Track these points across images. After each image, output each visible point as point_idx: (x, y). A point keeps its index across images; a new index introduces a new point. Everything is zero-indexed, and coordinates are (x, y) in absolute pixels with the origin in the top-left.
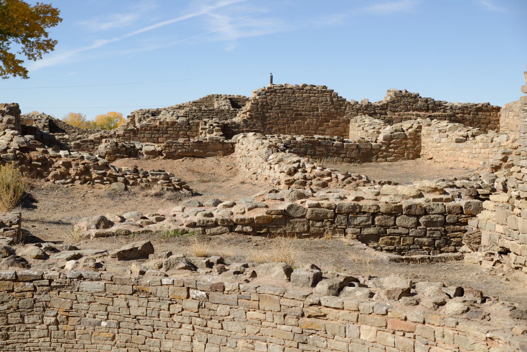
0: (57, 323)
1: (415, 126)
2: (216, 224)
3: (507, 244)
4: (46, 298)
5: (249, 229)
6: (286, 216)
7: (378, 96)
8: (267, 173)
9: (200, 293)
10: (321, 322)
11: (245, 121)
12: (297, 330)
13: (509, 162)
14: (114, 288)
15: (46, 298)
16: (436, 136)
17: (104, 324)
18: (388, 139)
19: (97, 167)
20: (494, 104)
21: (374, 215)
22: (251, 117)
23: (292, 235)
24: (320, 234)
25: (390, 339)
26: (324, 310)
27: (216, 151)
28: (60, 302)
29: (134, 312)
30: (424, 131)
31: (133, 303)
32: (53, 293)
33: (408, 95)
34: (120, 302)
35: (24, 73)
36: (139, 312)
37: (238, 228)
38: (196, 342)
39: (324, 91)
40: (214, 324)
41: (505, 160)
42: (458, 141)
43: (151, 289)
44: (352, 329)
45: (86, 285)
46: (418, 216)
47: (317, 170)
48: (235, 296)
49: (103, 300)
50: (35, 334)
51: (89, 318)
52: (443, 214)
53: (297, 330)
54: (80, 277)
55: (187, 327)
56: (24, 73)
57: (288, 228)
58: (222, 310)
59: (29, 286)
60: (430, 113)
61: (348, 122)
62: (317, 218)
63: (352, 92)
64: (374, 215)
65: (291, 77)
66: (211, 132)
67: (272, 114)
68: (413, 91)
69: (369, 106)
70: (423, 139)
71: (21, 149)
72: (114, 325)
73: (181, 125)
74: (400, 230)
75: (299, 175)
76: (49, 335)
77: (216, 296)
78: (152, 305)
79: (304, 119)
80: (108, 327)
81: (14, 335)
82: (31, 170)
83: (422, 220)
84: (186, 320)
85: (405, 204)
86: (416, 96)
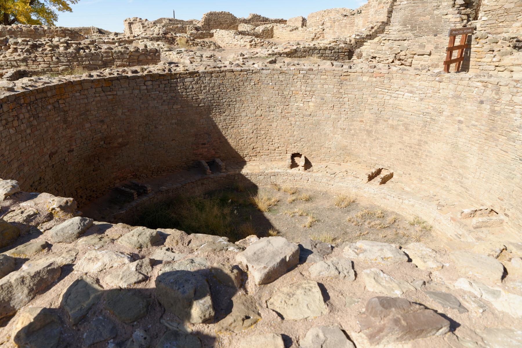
0: (255, 84)
1: (272, 26)
2: (276, 54)
3: (375, 55)
4: (251, 76)
5: (285, 55)
6: (296, 51)
7: (247, 17)
8: (236, 43)
9: (304, 72)
10: (348, 77)
11: (202, 26)
12: (340, 80)
13: (317, 37)
14: (274, 72)
15: (251, 76)
16: (281, 30)
17: (271, 84)
18: (263, 31)
19: (191, 40)
20: (285, 19)
21: (320, 50)
22: (205, 24)
23: (297, 57)
24: (305, 57)
25: (374, 79)
26: (349, 73)
27: (207, 36)
28: (256, 77)
29: (280, 79)
30: (275, 28)
31: (280, 77)
32: (254, 75)
33: (257, 16)
34: (276, 76)
35: (71, 10)
36: (282, 79)
37: (282, 55)
38: (302, 87)
39: (229, 14)
40: (309, 81)
41: (315, 36)
42: (290, 31)
43: (286, 72)
44: (360, 78)
45: (264, 71)
46: (332, 50)
47: (259, 41)
48: (317, 72)
49: (270, 76)
50: (248, 89)
51: (265, 82)
52: (338, 49)
53: (340, 80)
54: (263, 69)
55: (299, 83)
56: (71, 10)
57: (296, 55)
58: (312, 76)
59: (245, 73)
60: (265, 22)
61: (238, 26)
62: (305, 51)
63: (239, 15)
64: (320, 50)
65: (218, 9)
66: (192, 30)
67: (212, 23)
68: (259, 14)
69: (244, 20)
70: (274, 31)
71: (164, 33)
72: (274, 84)
73: (180, 27)
74: (327, 55)
75: (253, 43)
76: (252, 88)
77: (311, 72)
78: (287, 77)
79: (223, 25)
80: (272, 85)
81: (241, 89)
82: (169, 42)
83: (333, 51)
84: (299, 80)
85: (328, 46)
86: (260, 16)
